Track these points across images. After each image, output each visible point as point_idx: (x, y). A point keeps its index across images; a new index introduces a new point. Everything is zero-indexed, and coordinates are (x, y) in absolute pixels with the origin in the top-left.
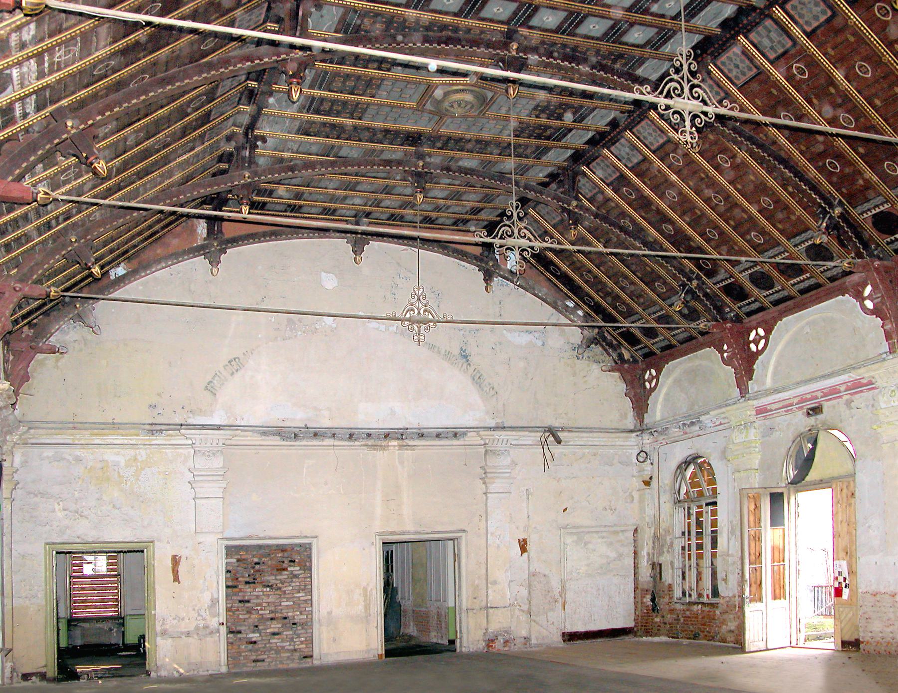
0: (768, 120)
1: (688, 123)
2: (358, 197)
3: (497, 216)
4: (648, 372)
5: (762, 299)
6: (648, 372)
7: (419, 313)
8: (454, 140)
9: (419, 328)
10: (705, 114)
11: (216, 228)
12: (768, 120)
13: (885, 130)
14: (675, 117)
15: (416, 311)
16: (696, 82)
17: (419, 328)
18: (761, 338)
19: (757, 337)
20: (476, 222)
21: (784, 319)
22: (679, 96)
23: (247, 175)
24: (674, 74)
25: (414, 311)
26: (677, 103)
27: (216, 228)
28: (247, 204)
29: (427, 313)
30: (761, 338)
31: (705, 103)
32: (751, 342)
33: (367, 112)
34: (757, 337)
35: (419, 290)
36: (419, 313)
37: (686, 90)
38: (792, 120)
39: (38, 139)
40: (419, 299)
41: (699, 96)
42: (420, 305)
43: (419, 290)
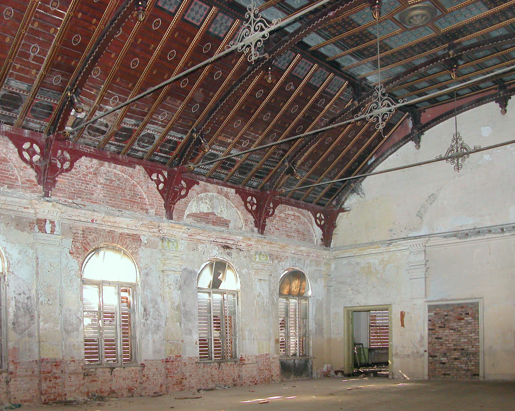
40: (457, 142)
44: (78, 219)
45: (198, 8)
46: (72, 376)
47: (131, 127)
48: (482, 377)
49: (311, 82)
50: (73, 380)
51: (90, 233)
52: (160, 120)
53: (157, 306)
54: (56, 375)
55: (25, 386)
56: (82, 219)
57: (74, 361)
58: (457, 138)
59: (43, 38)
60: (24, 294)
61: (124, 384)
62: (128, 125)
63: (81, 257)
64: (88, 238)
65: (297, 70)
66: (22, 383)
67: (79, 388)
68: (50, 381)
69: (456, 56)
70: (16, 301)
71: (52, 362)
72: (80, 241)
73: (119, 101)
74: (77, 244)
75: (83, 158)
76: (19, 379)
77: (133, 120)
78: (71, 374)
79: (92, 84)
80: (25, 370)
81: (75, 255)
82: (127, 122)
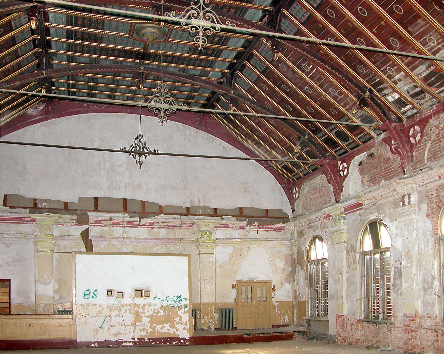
0: (321, 41)
1: (201, 34)
2: (180, 101)
3: (206, 101)
4: (295, 189)
5: (346, 147)
6: (295, 189)
7: (140, 149)
8: (182, 58)
9: (140, 157)
10: (214, 28)
11: (50, 108)
12: (321, 41)
13: (423, 52)
14: (193, 30)
15: (138, 148)
16: (208, 9)
17: (140, 157)
18: (345, 168)
19: (343, 168)
20: (195, 104)
21: (356, 157)
22: (196, 18)
23: (44, 73)
24: (193, 5)
25: (137, 147)
26: (194, 22)
27: (50, 108)
28: (45, 88)
29: (144, 149)
30: (345, 168)
31: (213, 22)
32: (340, 171)
33: (189, 49)
34: (343, 168)
35: (140, 136)
36: (140, 149)
37: (201, 14)
38: (363, 44)
39: (412, 154)
40: (140, 141)
41: (210, 18)
42: (141, 144)
43: (140, 136)
44: (429, 182)
45: (300, 14)
46: (428, 331)
47: (428, 72)
48: (185, 300)
49: (255, 57)
50: (429, 335)
51: (442, 189)
52: (435, 46)
53: (381, 258)
54: (412, 329)
55: (399, 335)
56: (432, 180)
57: (430, 317)
58: (140, 138)
59: (327, 83)
60: (399, 260)
61: (430, 339)
62: (424, 73)
63: (435, 217)
64: (441, 196)
65: (302, 10)
66: (398, 332)
67: (433, 344)
68: (409, 333)
69: (145, 73)
70: (395, 267)
71: (410, 317)
72: (435, 201)
73: (393, 68)
74: (432, 205)
75: (431, 121)
76: (396, 329)
77: (421, 67)
78: (427, 329)
79: (372, 76)
80: (399, 323)
81: (431, 216)
82: (419, 72)
